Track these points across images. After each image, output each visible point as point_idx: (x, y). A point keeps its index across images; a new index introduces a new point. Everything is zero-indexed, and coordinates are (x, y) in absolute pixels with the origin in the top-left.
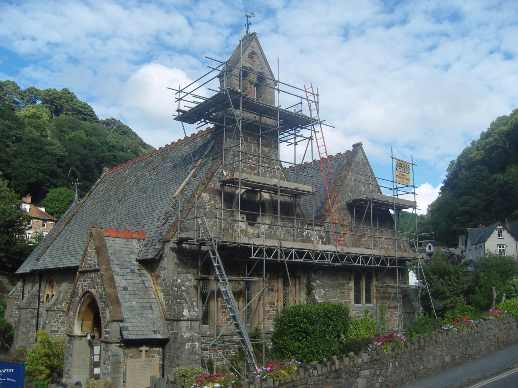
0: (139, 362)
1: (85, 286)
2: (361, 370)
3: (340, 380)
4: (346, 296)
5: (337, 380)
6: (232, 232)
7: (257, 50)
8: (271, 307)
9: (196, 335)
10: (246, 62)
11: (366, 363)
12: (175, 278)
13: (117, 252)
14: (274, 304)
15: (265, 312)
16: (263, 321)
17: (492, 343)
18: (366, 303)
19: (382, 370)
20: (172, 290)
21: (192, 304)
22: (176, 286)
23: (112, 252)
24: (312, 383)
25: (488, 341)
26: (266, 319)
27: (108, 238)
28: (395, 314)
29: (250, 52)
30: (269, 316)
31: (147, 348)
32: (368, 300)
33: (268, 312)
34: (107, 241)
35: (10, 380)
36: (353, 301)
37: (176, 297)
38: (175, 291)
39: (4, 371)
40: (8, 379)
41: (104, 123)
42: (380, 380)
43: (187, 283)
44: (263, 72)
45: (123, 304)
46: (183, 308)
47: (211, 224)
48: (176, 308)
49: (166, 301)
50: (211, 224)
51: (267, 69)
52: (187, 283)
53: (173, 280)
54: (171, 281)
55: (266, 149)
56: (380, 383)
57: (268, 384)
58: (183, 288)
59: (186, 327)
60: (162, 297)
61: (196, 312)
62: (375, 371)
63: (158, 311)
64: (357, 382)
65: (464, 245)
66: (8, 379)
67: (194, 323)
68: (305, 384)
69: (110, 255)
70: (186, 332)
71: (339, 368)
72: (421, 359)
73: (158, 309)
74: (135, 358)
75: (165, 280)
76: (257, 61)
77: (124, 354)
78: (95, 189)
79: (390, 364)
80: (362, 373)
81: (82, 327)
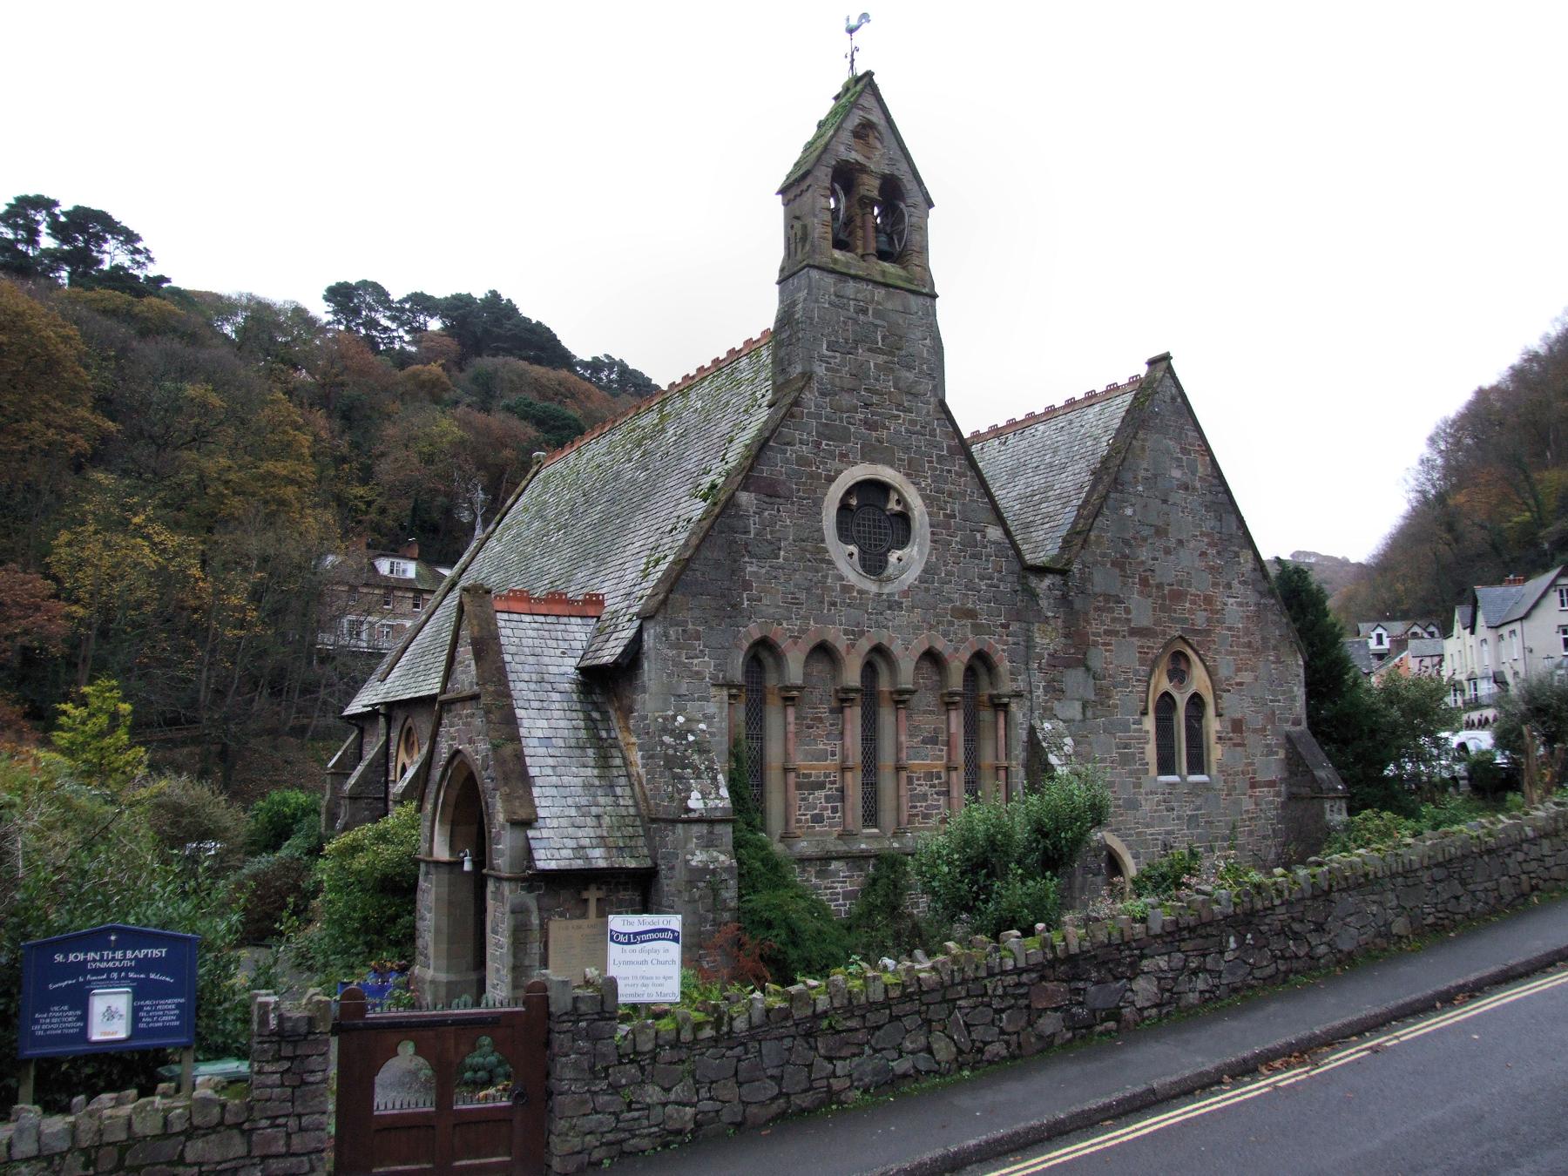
0: (579, 927)
1: (453, 739)
2: (1143, 957)
3: (1081, 985)
4: (1133, 754)
5: (1073, 985)
6: (819, 591)
7: (876, 117)
8: (931, 786)
9: (722, 858)
10: (849, 148)
11: (1156, 936)
12: (671, 713)
13: (526, 650)
14: (939, 777)
15: (913, 798)
16: (909, 822)
17: (1534, 882)
18: (1191, 771)
19: (1204, 956)
20: (662, 743)
21: (714, 779)
22: (671, 733)
23: (513, 649)
24: (1000, 991)
25: (1524, 877)
26: (917, 815)
27: (505, 616)
28: (1267, 803)
29: (857, 121)
30: (927, 808)
31: (601, 894)
32: (1197, 764)
33: (924, 797)
34: (501, 624)
35: (157, 977)
36: (1153, 768)
37: (670, 763)
38: (668, 746)
39: (141, 954)
40: (152, 976)
41: (585, 365)
42: (1201, 985)
43: (702, 726)
44: (896, 173)
45: (538, 781)
46: (689, 790)
47: (764, 571)
48: (670, 789)
49: (647, 774)
50: (764, 571)
51: (904, 166)
52: (702, 726)
53: (665, 719)
54: (660, 720)
55: (908, 374)
56: (1201, 992)
57: (871, 995)
58: (691, 738)
59: (697, 838)
60: (639, 762)
61: (722, 798)
62: (1186, 960)
63: (631, 797)
64: (1132, 990)
65: (1468, 630)
66: (152, 976)
67: (719, 829)
68: (977, 996)
69: (507, 658)
70: (698, 852)
71: (1077, 951)
72: (1320, 928)
73: (628, 791)
74: (571, 918)
75: (646, 718)
76: (878, 145)
77: (540, 909)
78: (512, 505)
79: (1228, 941)
80: (1146, 964)
81: (451, 841)
